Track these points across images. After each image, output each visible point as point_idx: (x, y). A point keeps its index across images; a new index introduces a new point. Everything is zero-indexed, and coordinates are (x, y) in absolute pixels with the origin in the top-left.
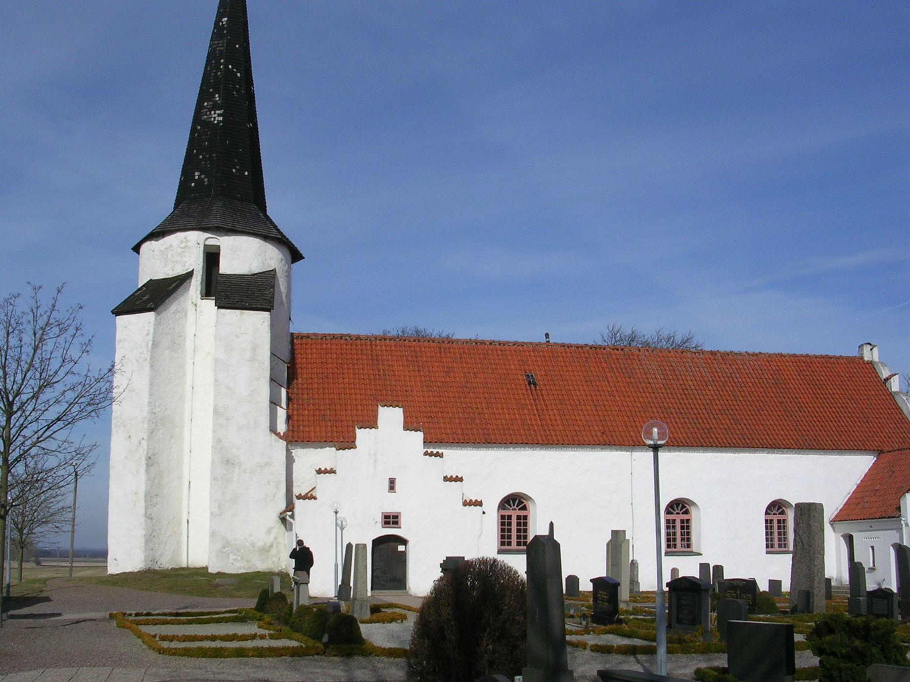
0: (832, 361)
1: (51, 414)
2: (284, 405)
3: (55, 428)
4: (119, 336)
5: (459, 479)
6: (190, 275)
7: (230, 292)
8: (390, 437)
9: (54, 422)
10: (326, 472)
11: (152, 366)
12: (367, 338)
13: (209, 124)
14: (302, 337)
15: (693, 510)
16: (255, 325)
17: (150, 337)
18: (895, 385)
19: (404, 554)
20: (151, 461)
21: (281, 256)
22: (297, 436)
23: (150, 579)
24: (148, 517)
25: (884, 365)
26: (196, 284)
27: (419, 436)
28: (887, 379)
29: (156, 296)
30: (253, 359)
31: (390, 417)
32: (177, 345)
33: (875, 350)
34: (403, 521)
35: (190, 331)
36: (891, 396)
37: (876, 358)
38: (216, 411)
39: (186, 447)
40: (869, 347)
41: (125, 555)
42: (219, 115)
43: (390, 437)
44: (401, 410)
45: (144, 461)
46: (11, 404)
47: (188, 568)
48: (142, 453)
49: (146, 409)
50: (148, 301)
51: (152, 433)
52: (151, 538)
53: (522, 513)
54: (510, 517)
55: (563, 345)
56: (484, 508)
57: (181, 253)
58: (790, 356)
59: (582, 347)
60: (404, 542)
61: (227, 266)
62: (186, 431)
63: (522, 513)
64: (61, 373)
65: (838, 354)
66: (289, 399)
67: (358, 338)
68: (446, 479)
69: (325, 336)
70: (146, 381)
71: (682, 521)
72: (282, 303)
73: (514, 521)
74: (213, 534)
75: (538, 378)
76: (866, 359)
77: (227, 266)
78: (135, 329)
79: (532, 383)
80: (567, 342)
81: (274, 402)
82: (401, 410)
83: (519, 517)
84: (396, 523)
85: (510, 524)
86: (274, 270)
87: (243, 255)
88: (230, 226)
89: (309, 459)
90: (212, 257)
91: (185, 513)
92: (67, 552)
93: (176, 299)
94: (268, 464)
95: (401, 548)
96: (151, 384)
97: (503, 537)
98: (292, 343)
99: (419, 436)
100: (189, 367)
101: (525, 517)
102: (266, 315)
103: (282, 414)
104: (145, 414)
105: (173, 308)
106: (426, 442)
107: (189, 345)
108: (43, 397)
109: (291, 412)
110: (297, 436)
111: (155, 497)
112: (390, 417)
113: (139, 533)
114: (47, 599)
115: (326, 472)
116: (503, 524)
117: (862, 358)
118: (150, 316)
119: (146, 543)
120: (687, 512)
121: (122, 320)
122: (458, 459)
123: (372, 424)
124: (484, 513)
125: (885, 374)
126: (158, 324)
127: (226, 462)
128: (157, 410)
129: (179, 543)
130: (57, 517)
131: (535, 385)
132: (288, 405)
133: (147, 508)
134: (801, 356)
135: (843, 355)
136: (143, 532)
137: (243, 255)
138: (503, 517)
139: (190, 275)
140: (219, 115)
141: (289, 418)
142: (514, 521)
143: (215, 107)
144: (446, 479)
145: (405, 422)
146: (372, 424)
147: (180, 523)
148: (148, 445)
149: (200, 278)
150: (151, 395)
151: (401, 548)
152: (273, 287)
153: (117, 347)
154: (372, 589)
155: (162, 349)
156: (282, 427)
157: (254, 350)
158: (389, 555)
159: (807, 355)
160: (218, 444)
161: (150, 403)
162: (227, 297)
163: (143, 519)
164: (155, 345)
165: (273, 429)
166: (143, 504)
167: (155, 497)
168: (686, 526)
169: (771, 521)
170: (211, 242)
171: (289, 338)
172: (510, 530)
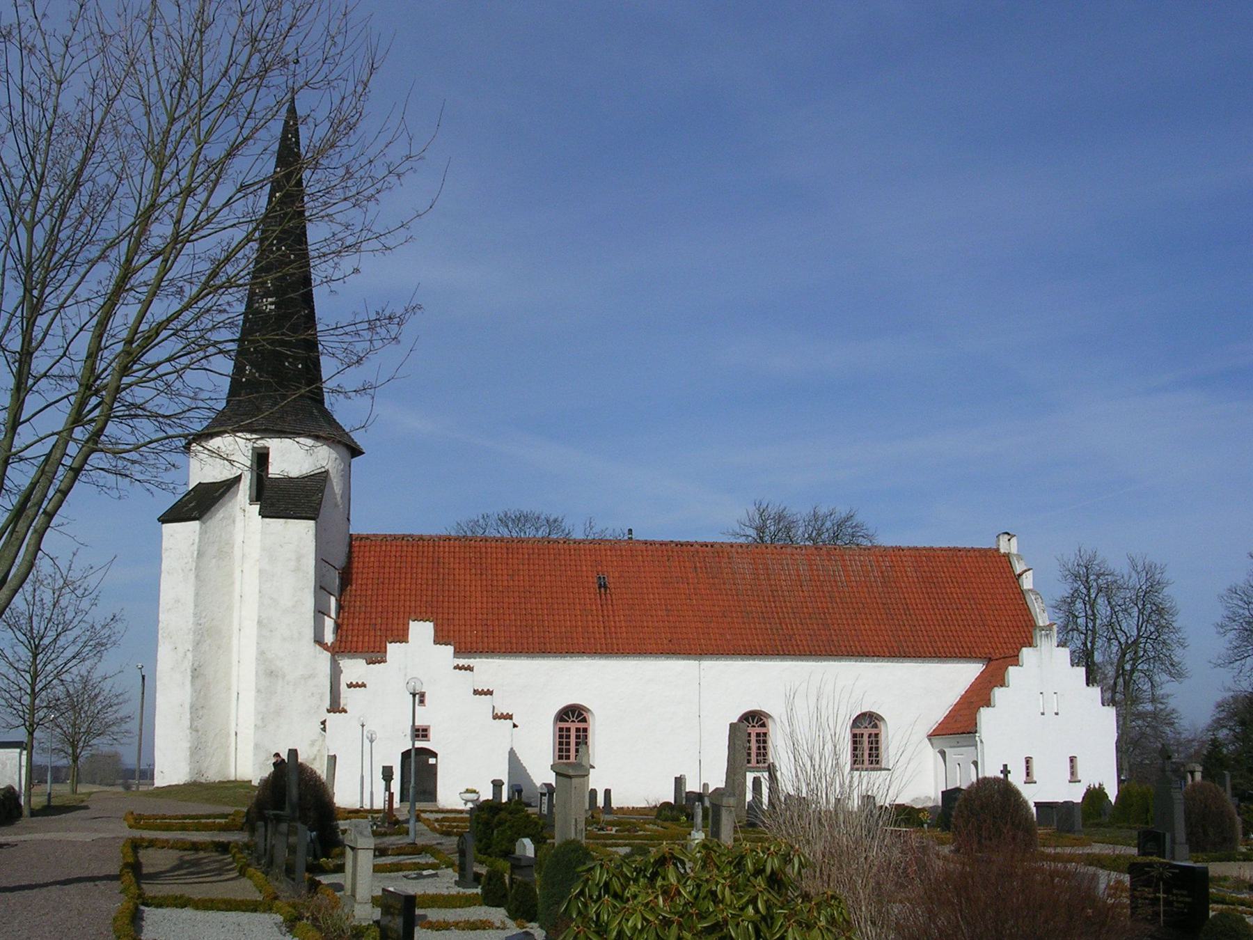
0: (972, 553)
1: (69, 653)
2: (333, 615)
3: (70, 665)
4: (165, 544)
5: (490, 693)
6: (238, 479)
7: (279, 499)
8: (420, 651)
9: (69, 661)
10: (357, 685)
11: (197, 576)
12: (431, 538)
13: (258, 311)
14: (361, 538)
15: (770, 723)
16: (299, 535)
17: (195, 547)
18: (1027, 583)
19: (435, 766)
20: (196, 673)
21: (334, 455)
22: (341, 649)
23: (193, 790)
24: (194, 729)
25: (1019, 557)
26: (244, 488)
27: (392, 648)
28: (1020, 575)
29: (201, 503)
30: (297, 569)
31: (421, 631)
32: (224, 554)
33: (1014, 540)
34: (432, 734)
35: (238, 537)
36: (1022, 594)
37: (1014, 550)
38: (259, 622)
39: (235, 658)
40: (1007, 537)
41: (171, 767)
42: (271, 304)
43: (420, 651)
44: (431, 625)
45: (189, 673)
46: (37, 647)
47: (236, 781)
48: (187, 665)
49: (191, 620)
50: (193, 509)
51: (197, 644)
52: (197, 751)
53: (582, 725)
54: (568, 730)
55: (646, 543)
56: (515, 720)
57: (226, 457)
58: (909, 549)
59: (666, 544)
60: (435, 755)
61: (276, 468)
62: (235, 642)
63: (582, 725)
64: (76, 621)
65: (968, 546)
66: (340, 607)
67: (421, 538)
68: (476, 692)
69: (385, 536)
70: (191, 593)
71: (758, 735)
72: (336, 505)
73: (573, 734)
74: (257, 746)
75: (611, 582)
76: (1002, 551)
77: (276, 468)
78: (181, 535)
79: (603, 586)
80: (650, 539)
81: (320, 612)
82: (431, 625)
83: (578, 730)
84: (426, 736)
85: (568, 737)
86: (327, 472)
87: (292, 457)
88: (278, 428)
89: (353, 668)
90: (261, 458)
91: (233, 725)
92: (134, 771)
93: (222, 506)
94: (312, 676)
95: (432, 761)
96: (197, 594)
97: (560, 750)
98: (350, 546)
99: (392, 648)
100: (237, 573)
101: (585, 730)
102: (312, 523)
103: (329, 624)
104: (190, 625)
105: (220, 515)
106: (458, 653)
107: (237, 552)
108: (59, 643)
109: (340, 621)
110: (341, 649)
111: (200, 711)
112: (421, 631)
113: (185, 745)
114: (86, 808)
115: (357, 685)
116: (561, 737)
117: (998, 550)
118: (195, 525)
119: (192, 755)
120: (763, 725)
121: (168, 528)
122: (489, 669)
123: (402, 637)
124: (515, 726)
125: (1018, 568)
126: (203, 533)
127: (270, 673)
128: (202, 621)
129: (227, 755)
130: (114, 729)
131: (605, 587)
132: (338, 614)
133: (192, 720)
134: (925, 549)
135: (976, 546)
136: (188, 745)
137: (292, 457)
138: (561, 730)
139: (238, 479)
140: (271, 304)
141: (338, 627)
142: (573, 734)
143: (267, 294)
144: (476, 692)
145: (436, 636)
146: (402, 637)
147: (228, 735)
148: (194, 656)
149: (248, 482)
150: (196, 606)
151: (432, 761)
152: (322, 491)
153: (164, 556)
154: (401, 801)
155: (206, 558)
156: (329, 638)
157: (298, 559)
158: (419, 769)
159: (931, 549)
160: (261, 653)
161: (195, 614)
162: (272, 505)
163: (188, 732)
164: (200, 554)
165: (319, 641)
166: (188, 716)
167: (200, 711)
168: (875, 741)
169: (568, 730)
170: (261, 443)
171: (347, 539)
172: (568, 744)
